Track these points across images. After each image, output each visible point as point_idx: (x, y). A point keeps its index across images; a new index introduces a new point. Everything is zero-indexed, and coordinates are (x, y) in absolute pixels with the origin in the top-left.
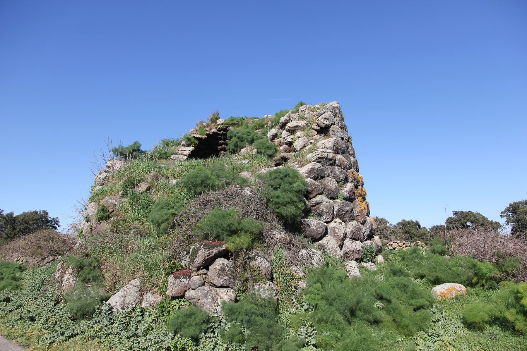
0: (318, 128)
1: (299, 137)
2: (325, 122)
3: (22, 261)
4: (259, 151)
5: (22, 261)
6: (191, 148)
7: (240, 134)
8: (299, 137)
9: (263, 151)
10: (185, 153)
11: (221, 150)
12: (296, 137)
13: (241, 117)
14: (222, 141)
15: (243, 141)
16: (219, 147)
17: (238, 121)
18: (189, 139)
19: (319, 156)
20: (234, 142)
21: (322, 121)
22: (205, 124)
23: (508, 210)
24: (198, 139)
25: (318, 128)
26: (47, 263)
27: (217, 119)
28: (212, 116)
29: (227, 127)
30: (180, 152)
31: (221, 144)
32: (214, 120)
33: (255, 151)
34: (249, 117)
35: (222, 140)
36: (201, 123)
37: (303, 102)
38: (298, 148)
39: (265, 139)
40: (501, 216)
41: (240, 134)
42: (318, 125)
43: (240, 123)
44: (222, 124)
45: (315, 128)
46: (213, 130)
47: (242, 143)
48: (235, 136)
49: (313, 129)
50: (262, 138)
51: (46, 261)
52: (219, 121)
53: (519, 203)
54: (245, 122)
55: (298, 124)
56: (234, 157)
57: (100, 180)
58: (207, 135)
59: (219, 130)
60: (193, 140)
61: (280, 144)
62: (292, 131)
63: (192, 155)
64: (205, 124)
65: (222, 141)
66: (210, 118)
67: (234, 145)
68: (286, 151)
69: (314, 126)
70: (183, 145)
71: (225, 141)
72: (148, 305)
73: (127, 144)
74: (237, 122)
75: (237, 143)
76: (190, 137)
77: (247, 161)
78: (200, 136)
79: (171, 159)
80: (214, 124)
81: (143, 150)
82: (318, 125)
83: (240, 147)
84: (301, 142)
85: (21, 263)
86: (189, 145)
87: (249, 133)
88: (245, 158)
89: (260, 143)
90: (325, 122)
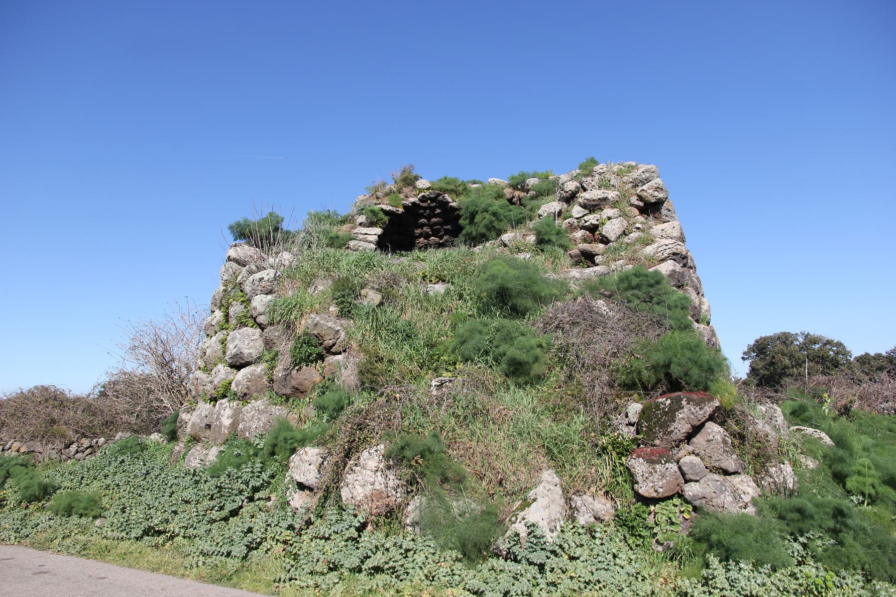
0: (641, 204)
1: (609, 218)
2: (656, 194)
3: (18, 451)
5: (18, 451)
6: (379, 231)
8: (609, 218)
10: (370, 238)
11: (420, 236)
12: (605, 217)
16: (418, 231)
19: (674, 250)
21: (650, 191)
23: (751, 349)
25: (641, 204)
26: (77, 452)
29: (439, 195)
30: (361, 237)
35: (425, 218)
37: (596, 158)
38: (612, 237)
40: (743, 358)
42: (640, 198)
44: (428, 189)
45: (637, 203)
46: (412, 200)
48: (486, 211)
49: (632, 205)
51: (74, 448)
53: (771, 338)
55: (606, 195)
57: (263, 284)
58: (405, 207)
59: (423, 199)
61: (572, 228)
62: (592, 207)
68: (585, 240)
69: (634, 200)
70: (361, 224)
71: (429, 220)
72: (592, 519)
73: (254, 215)
75: (491, 222)
78: (394, 209)
79: (348, 248)
80: (411, 188)
82: (640, 198)
84: (618, 226)
85: (14, 454)
86: (371, 224)
90: (656, 194)
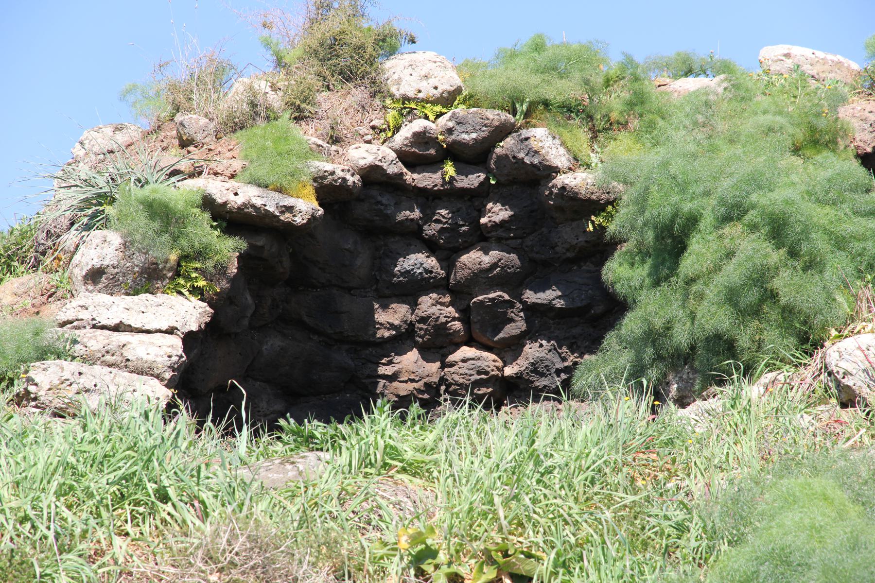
11: (404, 338)
14: (418, 261)
16: (391, 316)
30: (96, 341)
31: (411, 289)
35: (431, 246)
44: (448, 100)
48: (732, 213)
58: (329, 192)
59: (422, 153)
63: (205, 383)
65: (418, 261)
70: (95, 276)
80: (358, 94)
81: (195, 301)
86: (149, 278)
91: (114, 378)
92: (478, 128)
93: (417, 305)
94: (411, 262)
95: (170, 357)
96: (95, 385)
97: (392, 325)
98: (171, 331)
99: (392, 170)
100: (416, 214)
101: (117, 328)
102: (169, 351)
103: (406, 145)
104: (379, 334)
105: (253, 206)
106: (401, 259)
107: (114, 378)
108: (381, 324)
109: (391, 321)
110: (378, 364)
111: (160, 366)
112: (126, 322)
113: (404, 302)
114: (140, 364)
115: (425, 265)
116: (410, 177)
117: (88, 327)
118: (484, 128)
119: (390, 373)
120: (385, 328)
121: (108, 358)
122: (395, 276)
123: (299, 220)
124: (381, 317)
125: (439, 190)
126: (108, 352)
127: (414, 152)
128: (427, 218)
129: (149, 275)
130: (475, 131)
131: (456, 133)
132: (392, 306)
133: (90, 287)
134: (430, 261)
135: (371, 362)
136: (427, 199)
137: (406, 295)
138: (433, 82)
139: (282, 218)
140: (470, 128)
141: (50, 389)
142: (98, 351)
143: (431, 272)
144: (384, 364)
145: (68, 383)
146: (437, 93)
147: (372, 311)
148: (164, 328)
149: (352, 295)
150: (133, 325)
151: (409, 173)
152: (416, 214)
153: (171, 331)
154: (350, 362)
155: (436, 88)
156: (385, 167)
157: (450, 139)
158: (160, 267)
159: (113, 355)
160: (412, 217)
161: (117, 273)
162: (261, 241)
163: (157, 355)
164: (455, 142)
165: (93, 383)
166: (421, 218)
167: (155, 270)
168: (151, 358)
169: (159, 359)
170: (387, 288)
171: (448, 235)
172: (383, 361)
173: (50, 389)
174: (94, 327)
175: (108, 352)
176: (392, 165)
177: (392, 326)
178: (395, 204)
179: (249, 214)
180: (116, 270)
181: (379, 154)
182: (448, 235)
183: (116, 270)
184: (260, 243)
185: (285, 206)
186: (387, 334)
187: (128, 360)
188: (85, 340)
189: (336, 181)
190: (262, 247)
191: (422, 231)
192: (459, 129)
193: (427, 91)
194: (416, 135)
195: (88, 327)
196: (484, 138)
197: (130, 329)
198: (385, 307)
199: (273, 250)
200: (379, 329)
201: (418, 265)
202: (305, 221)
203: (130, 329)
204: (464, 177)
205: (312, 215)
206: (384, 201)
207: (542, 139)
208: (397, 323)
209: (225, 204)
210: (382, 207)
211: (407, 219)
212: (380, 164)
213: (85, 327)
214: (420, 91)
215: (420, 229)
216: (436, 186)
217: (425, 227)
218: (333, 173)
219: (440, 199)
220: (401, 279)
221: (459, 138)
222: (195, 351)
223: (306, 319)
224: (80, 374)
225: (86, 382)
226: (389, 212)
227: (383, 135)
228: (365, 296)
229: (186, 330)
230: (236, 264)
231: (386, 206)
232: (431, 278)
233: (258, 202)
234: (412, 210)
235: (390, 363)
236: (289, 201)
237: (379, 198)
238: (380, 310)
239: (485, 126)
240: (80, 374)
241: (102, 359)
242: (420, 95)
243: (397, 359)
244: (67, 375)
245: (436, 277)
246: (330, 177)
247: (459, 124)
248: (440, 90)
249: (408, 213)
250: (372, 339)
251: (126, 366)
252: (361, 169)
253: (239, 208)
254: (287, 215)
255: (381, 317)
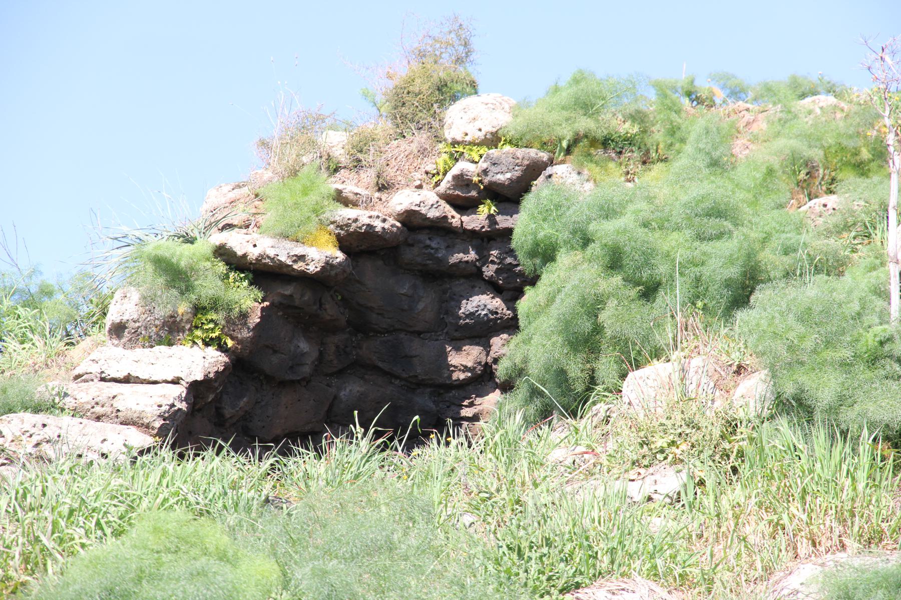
4: (789, 390)
6: (198, 361)
7: (626, 221)
9: (825, 388)
13: (681, 77)
14: (482, 303)
15: (649, 291)
16: (464, 359)
17: (638, 117)
18: (176, 276)
20: (564, 304)
22: (336, 142)
24: (263, 274)
27: (446, 93)
28: (402, 71)
30: (85, 394)
32: (422, 102)
33: (752, 391)
34: (752, 76)
35: (495, 288)
36: (307, 128)
39: (855, 282)
41: (626, 221)
43: (658, 135)
44: (493, 140)
46: (403, 200)
47: (641, 313)
50: (833, 267)
52: (464, 119)
54: (696, 122)
56: (559, 442)
60: (211, 282)
63: (205, 420)
64: (336, 142)
66: (382, 88)
67: (566, 325)
70: (118, 330)
74: (630, 128)
75: (593, 307)
76: (183, 254)
77: (668, 480)
78: (282, 252)
80: (422, 138)
83: (622, 344)
86: (171, 331)
87: (716, 216)
88: (649, 456)
89: (805, 317)
91: (84, 428)
92: (511, 167)
93: (490, 347)
94: (474, 304)
95: (160, 406)
96: (59, 436)
97: (466, 367)
98: (176, 381)
99: (433, 214)
100: (472, 255)
101: (127, 380)
102: (160, 401)
103: (449, 188)
104: (455, 376)
105: (269, 257)
106: (464, 302)
107: (84, 428)
108: (454, 366)
109: (464, 363)
110: (461, 406)
111: (149, 415)
112: (134, 374)
113: (477, 344)
114: (129, 414)
115: (489, 307)
116: (456, 219)
117: (96, 380)
118: (517, 168)
119: (470, 415)
120: (460, 370)
121: (98, 410)
122: (460, 318)
123: (312, 268)
124: (455, 359)
125: (486, 231)
126: (97, 404)
127: (458, 195)
128: (484, 258)
129: (170, 328)
130: (509, 171)
131: (490, 174)
132: (464, 348)
133: (116, 342)
134: (494, 301)
135: (454, 404)
136: (482, 240)
137: (480, 337)
138: (478, 124)
139: (295, 267)
140: (504, 169)
141: (13, 441)
142: (88, 403)
143: (497, 313)
144: (466, 406)
145: (28, 434)
146: (481, 135)
147: (445, 355)
148: (169, 379)
149: (423, 339)
150: (141, 377)
151: (458, 216)
152: (472, 255)
153: (176, 381)
154: (432, 405)
155: (480, 130)
156: (423, 212)
157: (486, 180)
158: (178, 319)
159: (103, 406)
160: (466, 259)
161: (139, 327)
162: (288, 290)
163: (146, 406)
164: (491, 183)
165: (56, 434)
166: (477, 260)
167: (174, 322)
168: (139, 408)
169: (148, 410)
170: (456, 331)
171: (506, 275)
172: (465, 403)
173: (13, 441)
174: (103, 379)
175: (97, 404)
176: (433, 209)
177: (466, 369)
178: (448, 247)
179: (265, 264)
180: (137, 324)
181: (428, 201)
182: (506, 275)
183: (137, 324)
184: (288, 293)
185: (296, 256)
186: (462, 376)
187: (118, 411)
188: (75, 393)
189: (360, 228)
190: (291, 296)
191: (482, 273)
192: (494, 169)
193: (475, 135)
194: (455, 178)
195: (96, 380)
196: (518, 177)
197: (138, 381)
198: (458, 349)
199: (306, 298)
200: (453, 371)
201: (482, 307)
202: (318, 269)
203: (138, 381)
204: (509, 217)
205: (327, 263)
206: (434, 244)
207: (564, 176)
208: (470, 365)
209: (245, 256)
210: (432, 251)
211: (460, 262)
212: (417, 208)
213: (92, 380)
214: (467, 134)
215: (480, 273)
216: (483, 227)
217: (484, 269)
218: (356, 220)
219: (494, 240)
220: (467, 321)
221: (494, 179)
222: (245, 399)
223: (380, 364)
224: (44, 425)
225: (50, 432)
226: (440, 255)
227: (435, 179)
228: (437, 340)
229: (190, 379)
230: (259, 314)
231: (437, 249)
232: (497, 319)
233: (271, 253)
234: (466, 252)
235: (471, 405)
236: (299, 250)
237: (428, 242)
238: (453, 353)
239: (517, 165)
240: (44, 425)
241: (92, 410)
242: (468, 138)
243: (478, 401)
244: (27, 427)
245: (501, 318)
246: (354, 224)
247: (494, 164)
248: (483, 133)
249: (461, 255)
250: (447, 382)
251: (117, 417)
252: (398, 215)
253: (257, 259)
254: (301, 264)
255: (455, 359)
